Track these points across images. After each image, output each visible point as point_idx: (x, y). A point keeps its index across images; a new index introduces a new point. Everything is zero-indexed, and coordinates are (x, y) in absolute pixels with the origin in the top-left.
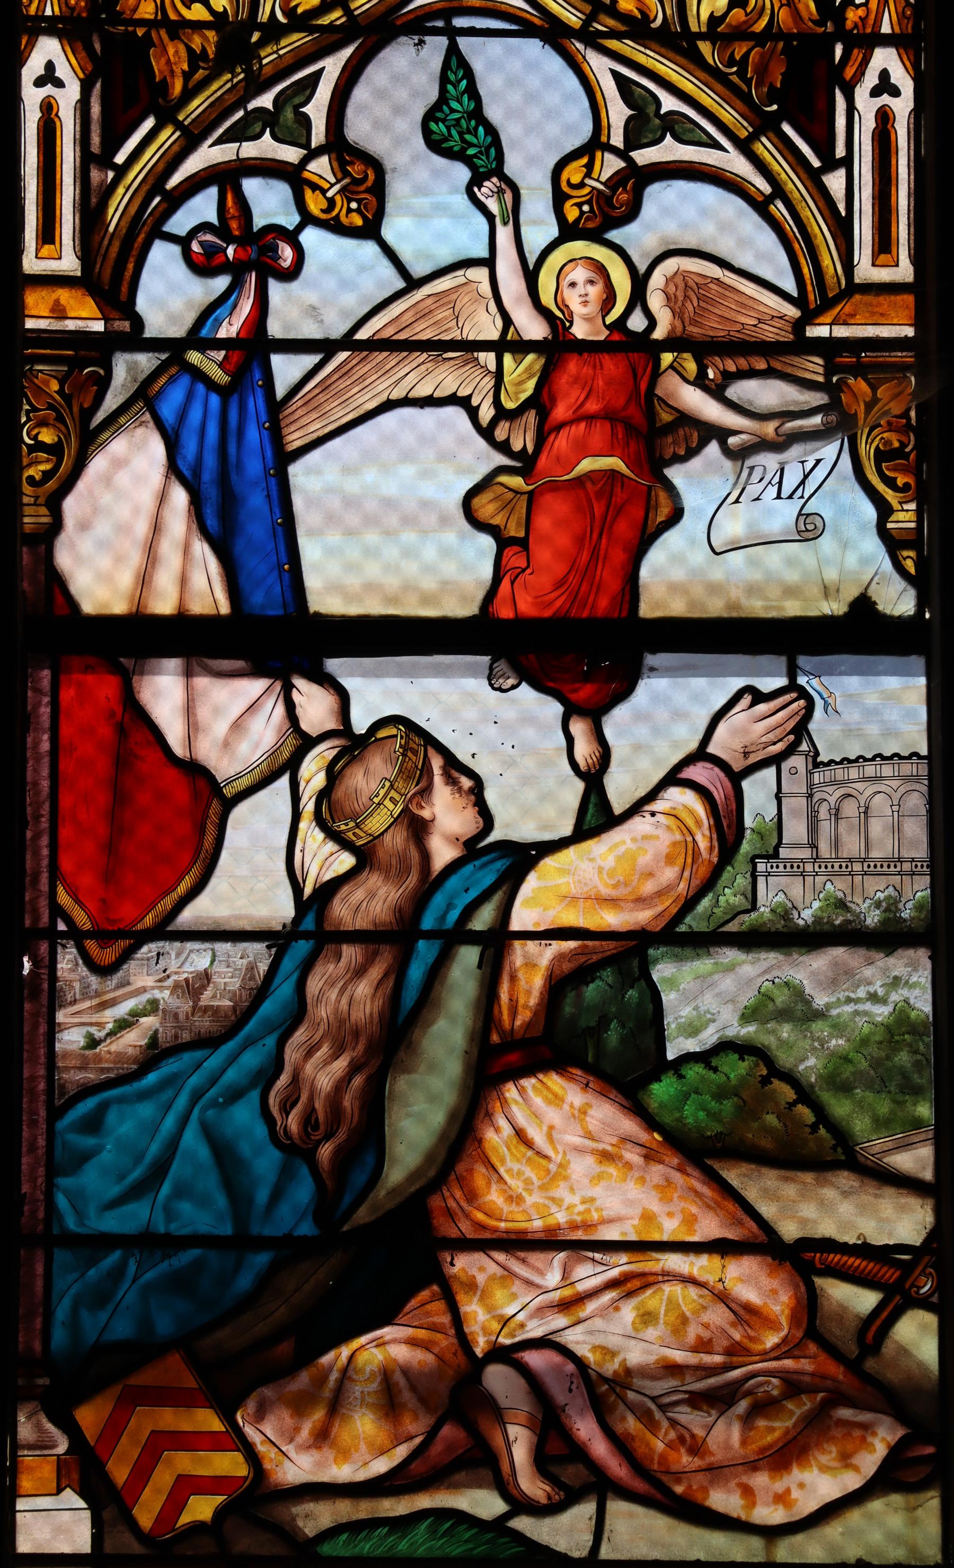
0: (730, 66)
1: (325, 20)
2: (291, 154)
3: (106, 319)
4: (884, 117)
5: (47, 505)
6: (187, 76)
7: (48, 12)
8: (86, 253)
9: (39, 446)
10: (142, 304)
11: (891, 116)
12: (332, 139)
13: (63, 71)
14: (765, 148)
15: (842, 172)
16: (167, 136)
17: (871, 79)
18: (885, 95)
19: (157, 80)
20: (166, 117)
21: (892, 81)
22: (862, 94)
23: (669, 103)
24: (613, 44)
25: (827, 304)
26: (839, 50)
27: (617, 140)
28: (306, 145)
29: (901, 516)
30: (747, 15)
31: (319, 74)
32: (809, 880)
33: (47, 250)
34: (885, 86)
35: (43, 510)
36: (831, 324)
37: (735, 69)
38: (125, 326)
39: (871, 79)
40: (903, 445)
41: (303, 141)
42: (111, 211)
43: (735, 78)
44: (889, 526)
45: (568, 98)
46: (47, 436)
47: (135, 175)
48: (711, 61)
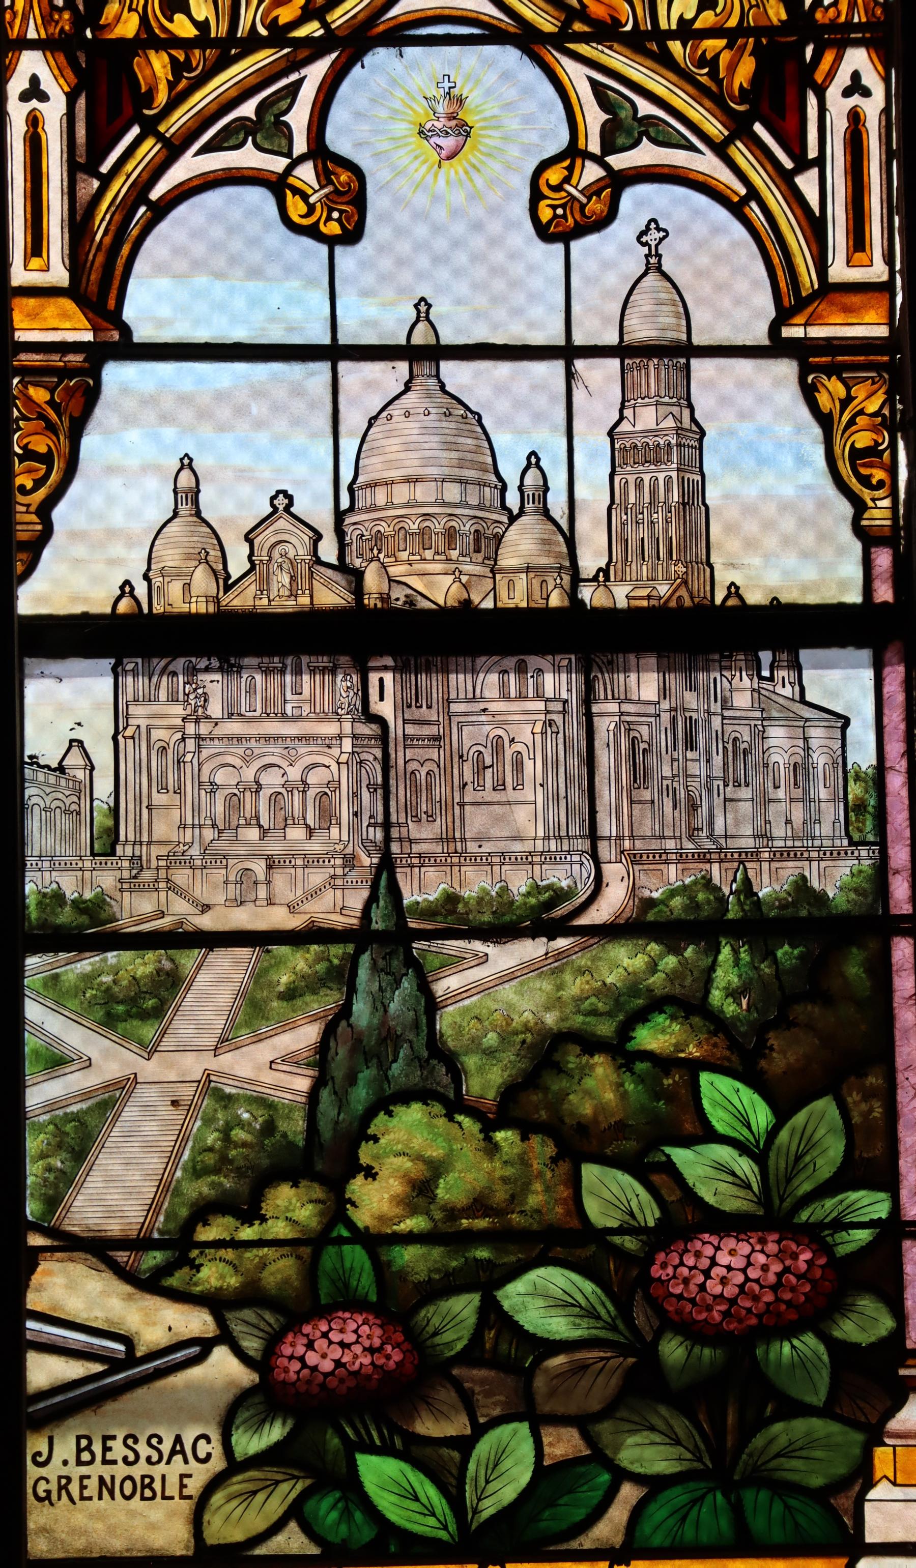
0: (700, 67)
1: (301, 32)
2: (279, 164)
3: (95, 329)
4: (855, 117)
5: (37, 513)
6: (171, 85)
7: (856, 20)
8: (76, 263)
9: (29, 455)
10: (129, 314)
11: (862, 117)
12: (313, 146)
13: (48, 83)
14: (740, 153)
15: (814, 172)
16: (149, 149)
17: (843, 79)
18: (34, 101)
19: (143, 90)
20: (150, 128)
21: (42, 87)
22: (833, 93)
23: (645, 108)
24: (583, 49)
25: (801, 303)
26: (809, 51)
27: (594, 147)
28: (289, 155)
29: (876, 513)
30: (716, 15)
31: (299, 83)
32: (496, 869)
33: (35, 263)
34: (856, 87)
35: (34, 518)
36: (806, 325)
37: (706, 70)
38: (116, 336)
39: (843, 79)
40: (877, 444)
41: (285, 150)
42: (97, 223)
43: (704, 80)
44: (864, 523)
45: (544, 106)
46: (40, 445)
47: (119, 187)
48: (683, 65)
